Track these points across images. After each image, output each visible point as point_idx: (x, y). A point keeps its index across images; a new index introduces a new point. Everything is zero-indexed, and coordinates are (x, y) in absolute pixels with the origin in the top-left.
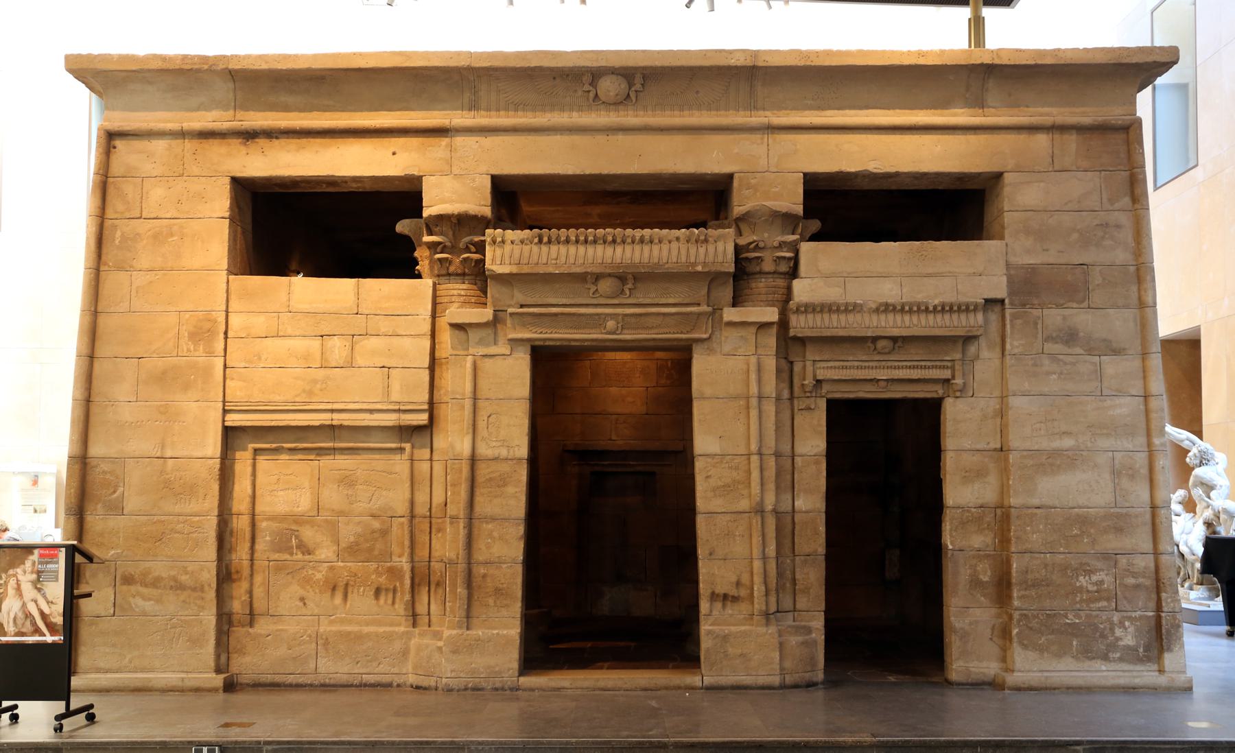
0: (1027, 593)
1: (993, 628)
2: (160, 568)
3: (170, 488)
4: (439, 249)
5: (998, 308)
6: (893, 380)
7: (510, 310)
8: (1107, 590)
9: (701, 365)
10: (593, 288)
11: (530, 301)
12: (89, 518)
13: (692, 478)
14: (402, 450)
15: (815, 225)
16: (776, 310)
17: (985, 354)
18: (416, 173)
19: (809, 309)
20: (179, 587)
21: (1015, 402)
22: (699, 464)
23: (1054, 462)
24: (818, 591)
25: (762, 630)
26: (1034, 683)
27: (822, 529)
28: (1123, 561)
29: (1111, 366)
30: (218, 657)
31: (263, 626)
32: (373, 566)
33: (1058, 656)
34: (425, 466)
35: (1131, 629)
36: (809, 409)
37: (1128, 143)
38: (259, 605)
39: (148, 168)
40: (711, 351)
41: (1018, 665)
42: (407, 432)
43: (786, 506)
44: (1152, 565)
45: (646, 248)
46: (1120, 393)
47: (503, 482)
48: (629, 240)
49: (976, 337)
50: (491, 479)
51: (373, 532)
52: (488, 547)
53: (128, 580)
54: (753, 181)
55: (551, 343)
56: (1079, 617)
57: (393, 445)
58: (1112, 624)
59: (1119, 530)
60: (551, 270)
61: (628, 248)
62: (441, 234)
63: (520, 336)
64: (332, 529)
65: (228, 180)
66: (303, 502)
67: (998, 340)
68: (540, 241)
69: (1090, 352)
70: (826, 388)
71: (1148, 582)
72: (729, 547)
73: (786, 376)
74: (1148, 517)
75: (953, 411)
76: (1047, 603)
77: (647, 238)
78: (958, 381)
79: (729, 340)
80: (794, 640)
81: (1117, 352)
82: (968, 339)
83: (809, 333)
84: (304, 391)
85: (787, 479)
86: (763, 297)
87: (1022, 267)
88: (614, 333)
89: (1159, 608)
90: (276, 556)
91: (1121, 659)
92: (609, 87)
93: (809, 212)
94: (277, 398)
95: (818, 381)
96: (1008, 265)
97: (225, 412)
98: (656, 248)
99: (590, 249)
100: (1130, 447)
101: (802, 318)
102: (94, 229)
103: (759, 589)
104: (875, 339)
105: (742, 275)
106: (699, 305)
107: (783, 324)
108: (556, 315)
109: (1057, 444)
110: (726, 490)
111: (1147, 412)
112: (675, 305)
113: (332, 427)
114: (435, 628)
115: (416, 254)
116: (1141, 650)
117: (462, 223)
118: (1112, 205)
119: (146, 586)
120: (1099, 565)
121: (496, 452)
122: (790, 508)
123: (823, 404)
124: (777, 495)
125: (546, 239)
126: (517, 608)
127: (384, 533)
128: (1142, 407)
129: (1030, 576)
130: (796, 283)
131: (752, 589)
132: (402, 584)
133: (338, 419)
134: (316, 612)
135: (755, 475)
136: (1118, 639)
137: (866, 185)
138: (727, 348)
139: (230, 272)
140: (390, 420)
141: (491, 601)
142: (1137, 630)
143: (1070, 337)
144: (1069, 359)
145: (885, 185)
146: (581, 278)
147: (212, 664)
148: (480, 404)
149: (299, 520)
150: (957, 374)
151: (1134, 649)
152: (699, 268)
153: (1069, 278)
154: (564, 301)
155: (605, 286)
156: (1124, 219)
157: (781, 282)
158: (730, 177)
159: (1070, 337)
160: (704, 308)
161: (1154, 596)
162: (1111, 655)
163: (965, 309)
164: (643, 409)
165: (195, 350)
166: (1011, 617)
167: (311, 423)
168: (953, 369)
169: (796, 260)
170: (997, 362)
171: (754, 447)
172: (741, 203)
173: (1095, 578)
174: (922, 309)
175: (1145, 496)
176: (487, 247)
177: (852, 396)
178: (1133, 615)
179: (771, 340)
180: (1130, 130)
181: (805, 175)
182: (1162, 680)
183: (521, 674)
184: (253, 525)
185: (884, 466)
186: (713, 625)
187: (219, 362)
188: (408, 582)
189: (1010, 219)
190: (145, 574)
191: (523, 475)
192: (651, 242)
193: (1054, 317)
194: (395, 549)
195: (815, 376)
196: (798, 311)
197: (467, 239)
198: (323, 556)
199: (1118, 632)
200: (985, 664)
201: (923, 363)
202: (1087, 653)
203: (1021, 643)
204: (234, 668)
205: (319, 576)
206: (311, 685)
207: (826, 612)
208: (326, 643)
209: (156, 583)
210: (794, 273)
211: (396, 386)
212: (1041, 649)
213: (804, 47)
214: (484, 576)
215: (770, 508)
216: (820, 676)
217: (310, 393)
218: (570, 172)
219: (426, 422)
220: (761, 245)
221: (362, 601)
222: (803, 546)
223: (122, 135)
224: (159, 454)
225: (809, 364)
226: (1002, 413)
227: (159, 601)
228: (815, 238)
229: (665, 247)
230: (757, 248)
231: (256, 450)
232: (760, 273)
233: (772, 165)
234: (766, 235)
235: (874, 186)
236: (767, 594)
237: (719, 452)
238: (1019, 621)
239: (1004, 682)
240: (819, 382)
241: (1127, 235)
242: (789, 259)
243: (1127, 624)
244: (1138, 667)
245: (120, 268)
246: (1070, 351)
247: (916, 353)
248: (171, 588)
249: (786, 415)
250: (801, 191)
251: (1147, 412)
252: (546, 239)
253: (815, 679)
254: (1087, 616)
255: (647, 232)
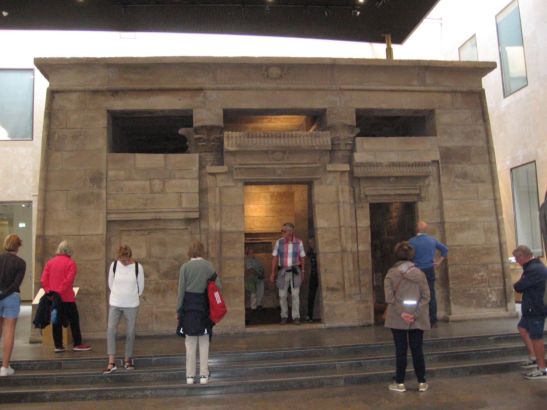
1: (442, 297)
6: (396, 195)
7: (235, 167)
8: (485, 279)
10: (271, 157)
11: (243, 162)
17: (432, 183)
18: (190, 108)
19: (362, 165)
21: (445, 202)
23: (463, 227)
26: (460, 319)
28: (490, 266)
29: (482, 188)
35: (495, 294)
36: (362, 207)
40: (321, 183)
41: (453, 312)
42: (189, 221)
44: (501, 268)
45: (294, 139)
48: (286, 136)
49: (428, 176)
58: (487, 291)
59: (488, 254)
60: (253, 149)
63: (239, 178)
69: (473, 182)
70: (368, 199)
71: (500, 275)
74: (498, 248)
77: (294, 135)
79: (330, 178)
80: (362, 306)
81: (482, 182)
82: (426, 177)
84: (143, 204)
91: (492, 307)
92: (274, 72)
93: (358, 126)
94: (131, 207)
97: (108, 213)
100: (490, 220)
106: (316, 163)
107: (351, 172)
108: (255, 168)
109: (462, 220)
110: (331, 243)
112: (305, 164)
113: (155, 220)
117: (211, 129)
121: (231, 229)
131: (344, 284)
133: (158, 216)
136: (490, 299)
138: (328, 182)
140: (182, 216)
141: (231, 295)
143: (464, 176)
146: (266, 152)
151: (497, 302)
152: (317, 148)
154: (258, 162)
158: (325, 110)
159: (464, 176)
161: (502, 280)
162: (488, 305)
167: (147, 218)
172: (330, 120)
173: (480, 274)
174: (408, 165)
175: (497, 240)
179: (346, 178)
180: (481, 94)
187: (104, 192)
192: (296, 137)
193: (458, 168)
197: (213, 136)
199: (490, 296)
202: (479, 305)
212: (462, 305)
213: (354, 57)
214: (228, 284)
216: (372, 321)
217: (146, 205)
219: (198, 217)
223: (57, 92)
224: (77, 234)
240: (366, 196)
241: (483, 135)
243: (493, 292)
245: (58, 150)
254: (478, 290)
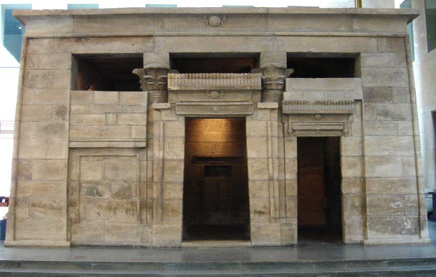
0: (372, 210)
1: (360, 223)
2: (46, 201)
3: (50, 170)
4: (150, 80)
5: (360, 103)
7: (177, 103)
9: (250, 125)
10: (208, 95)
12: (19, 182)
13: (246, 168)
14: (136, 156)
15: (291, 71)
16: (277, 103)
19: (290, 103)
20: (52, 208)
22: (249, 162)
23: (381, 160)
24: (295, 210)
25: (274, 224)
27: (296, 186)
28: (406, 197)
29: (401, 124)
30: (67, 235)
31: (83, 224)
32: (125, 201)
33: (385, 232)
34: (145, 163)
35: (410, 222)
36: (290, 141)
37: (405, 43)
38: (82, 215)
39: (42, 51)
40: (253, 119)
43: (282, 177)
44: (417, 198)
45: (228, 80)
46: (404, 135)
47: (175, 168)
49: (351, 114)
50: (170, 168)
51: (125, 188)
52: (169, 194)
53: (34, 205)
54: (268, 55)
55: (193, 116)
56: (391, 218)
57: (133, 155)
59: (405, 186)
61: (221, 80)
62: (152, 75)
63: (180, 113)
64: (109, 186)
65: (70, 56)
66: (98, 176)
67: (360, 115)
68: (189, 78)
69: (394, 119)
70: (297, 133)
71: (416, 205)
72: (260, 194)
73: (281, 128)
74: (415, 180)
75: (344, 141)
76: (380, 213)
78: (346, 130)
80: (286, 228)
81: (403, 119)
82: (349, 115)
83: (290, 112)
85: (283, 168)
86: (272, 99)
87: (368, 87)
88: (216, 112)
89: (419, 214)
90: (88, 197)
91: (406, 234)
93: (289, 66)
95: (294, 130)
96: (363, 87)
98: (232, 80)
99: (207, 80)
100: (408, 154)
101: (287, 106)
102: (21, 73)
103: (272, 209)
104: (315, 115)
105: (264, 89)
108: (194, 105)
109: (382, 154)
110: (260, 171)
111: (414, 142)
113: (109, 148)
114: (148, 224)
115: (140, 82)
116: (413, 230)
118: (399, 65)
119: (40, 207)
120: (398, 199)
122: (284, 179)
123: (295, 139)
124: (279, 173)
125: (190, 77)
126: (180, 217)
127: (129, 188)
128: (412, 140)
129: (373, 203)
130: (284, 93)
131: (270, 209)
132: (137, 207)
133: (111, 144)
134: (104, 218)
135: (271, 166)
136: (406, 226)
137: (310, 56)
139: (71, 89)
140: (131, 145)
141: (170, 214)
142: (412, 222)
143: (386, 114)
144: (387, 122)
145: (317, 56)
146: (204, 91)
147: (65, 237)
148: (166, 139)
149: (97, 183)
150: (345, 128)
152: (248, 88)
153: (385, 92)
155: (214, 94)
156: (405, 70)
157: (278, 92)
158: (259, 54)
159: (386, 114)
160: (250, 103)
162: (403, 232)
163: (347, 103)
164: (226, 141)
165: (58, 119)
166: (366, 219)
168: (344, 125)
169: (284, 85)
170: (360, 123)
171: (270, 155)
172: (264, 63)
173: (396, 204)
175: (414, 173)
176: (168, 80)
177: (306, 136)
178: (410, 217)
179: (275, 115)
181: (287, 53)
182: (420, 241)
183: (182, 242)
184: (80, 185)
185: (320, 161)
186: (255, 222)
188: (139, 207)
189: (364, 70)
190: (40, 203)
191: (182, 167)
193: (380, 106)
194: (134, 194)
195: (292, 128)
196: (286, 104)
198: (106, 197)
199: (405, 224)
200: (357, 237)
201: (312, 124)
202: (394, 231)
203: (370, 229)
204: (73, 240)
205: (104, 204)
206: (102, 246)
207: (298, 218)
208: (108, 230)
209: (44, 206)
210: (284, 89)
211: (134, 132)
212: (378, 231)
214: (168, 205)
215: (276, 178)
216: (296, 242)
218: (199, 52)
220: (271, 79)
221: (121, 216)
222: (289, 193)
224: (45, 158)
225: (290, 124)
226: (362, 142)
227: (45, 213)
228: (292, 76)
229: (235, 80)
230: (270, 80)
231: (81, 156)
232: (271, 89)
233: (275, 50)
234: (273, 75)
235: (314, 57)
236: (275, 210)
237: (256, 157)
238: (369, 220)
239: (364, 243)
242: (282, 84)
243: (408, 220)
244: (412, 236)
246: (386, 119)
247: (330, 120)
248: (50, 208)
249: (282, 144)
250: (286, 59)
251: (414, 142)
252: (190, 77)
253: (294, 243)
255: (228, 74)
